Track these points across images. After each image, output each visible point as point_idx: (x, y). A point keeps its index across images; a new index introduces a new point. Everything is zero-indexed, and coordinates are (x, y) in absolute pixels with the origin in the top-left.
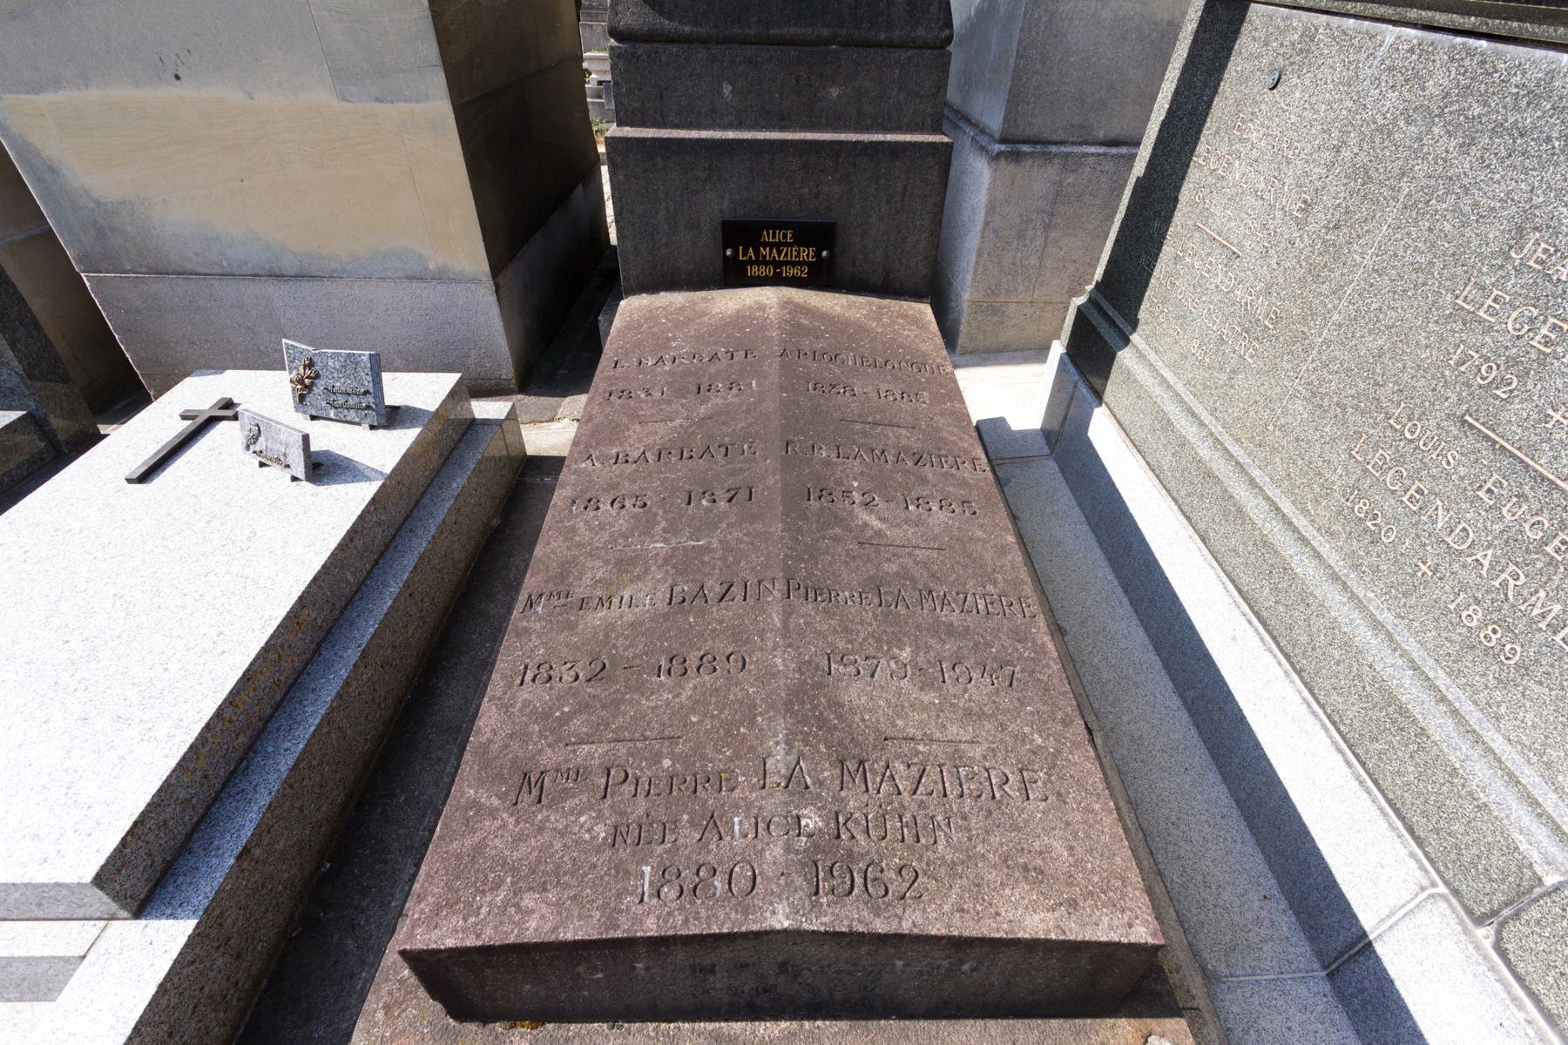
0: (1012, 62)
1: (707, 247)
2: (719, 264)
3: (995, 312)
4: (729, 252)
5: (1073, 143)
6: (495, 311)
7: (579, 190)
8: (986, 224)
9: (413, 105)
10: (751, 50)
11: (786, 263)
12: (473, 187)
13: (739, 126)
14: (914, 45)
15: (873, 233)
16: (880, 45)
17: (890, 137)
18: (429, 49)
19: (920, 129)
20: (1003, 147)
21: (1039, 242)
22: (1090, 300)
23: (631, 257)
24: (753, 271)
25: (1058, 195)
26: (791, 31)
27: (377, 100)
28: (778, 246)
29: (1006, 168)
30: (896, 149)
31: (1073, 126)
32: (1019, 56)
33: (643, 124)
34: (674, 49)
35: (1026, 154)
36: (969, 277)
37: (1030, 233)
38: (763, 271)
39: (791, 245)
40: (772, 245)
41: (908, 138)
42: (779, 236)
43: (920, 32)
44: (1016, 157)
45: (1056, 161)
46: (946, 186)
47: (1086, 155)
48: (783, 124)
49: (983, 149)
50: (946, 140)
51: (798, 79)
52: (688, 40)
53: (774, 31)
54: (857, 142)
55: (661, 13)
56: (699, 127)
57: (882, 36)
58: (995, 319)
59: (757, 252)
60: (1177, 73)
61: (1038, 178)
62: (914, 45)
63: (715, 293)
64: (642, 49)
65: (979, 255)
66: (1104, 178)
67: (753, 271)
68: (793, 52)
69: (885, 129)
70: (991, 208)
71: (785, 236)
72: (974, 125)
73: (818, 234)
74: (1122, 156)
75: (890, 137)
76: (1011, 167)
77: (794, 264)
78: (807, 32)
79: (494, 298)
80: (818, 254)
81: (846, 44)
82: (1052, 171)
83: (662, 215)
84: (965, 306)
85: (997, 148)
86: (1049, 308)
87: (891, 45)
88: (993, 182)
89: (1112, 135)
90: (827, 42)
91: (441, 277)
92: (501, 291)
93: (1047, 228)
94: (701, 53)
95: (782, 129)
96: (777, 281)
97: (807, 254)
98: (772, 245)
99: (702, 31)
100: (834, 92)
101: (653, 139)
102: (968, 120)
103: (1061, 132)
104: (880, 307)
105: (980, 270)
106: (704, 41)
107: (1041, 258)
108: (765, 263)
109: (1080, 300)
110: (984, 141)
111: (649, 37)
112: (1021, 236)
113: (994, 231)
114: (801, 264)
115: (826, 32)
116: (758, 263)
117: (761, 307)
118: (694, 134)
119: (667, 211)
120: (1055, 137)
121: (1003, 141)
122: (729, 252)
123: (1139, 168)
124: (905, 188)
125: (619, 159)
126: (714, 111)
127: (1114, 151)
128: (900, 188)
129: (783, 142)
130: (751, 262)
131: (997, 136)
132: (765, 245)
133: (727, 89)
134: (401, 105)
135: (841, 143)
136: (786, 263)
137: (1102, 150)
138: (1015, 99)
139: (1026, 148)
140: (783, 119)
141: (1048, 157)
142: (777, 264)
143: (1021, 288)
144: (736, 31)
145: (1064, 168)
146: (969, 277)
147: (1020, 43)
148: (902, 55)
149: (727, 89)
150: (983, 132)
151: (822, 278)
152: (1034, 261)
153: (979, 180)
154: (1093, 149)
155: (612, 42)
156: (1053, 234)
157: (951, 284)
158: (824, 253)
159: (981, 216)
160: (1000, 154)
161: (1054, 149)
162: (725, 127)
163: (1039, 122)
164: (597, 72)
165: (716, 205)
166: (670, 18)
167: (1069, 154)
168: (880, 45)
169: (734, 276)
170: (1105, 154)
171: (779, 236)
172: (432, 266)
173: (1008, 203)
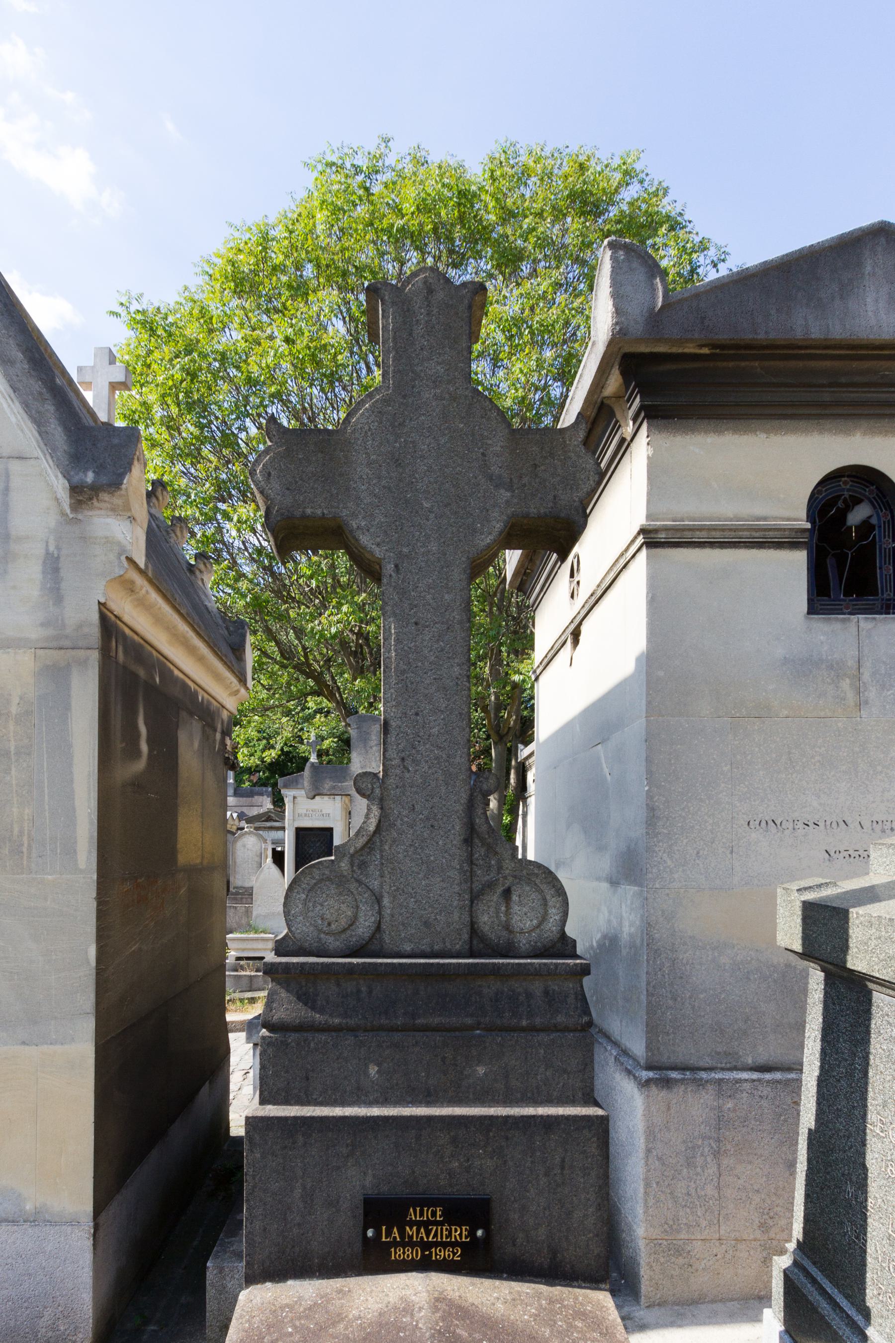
0: (643, 998)
1: (344, 1225)
2: (358, 1246)
3: (679, 1252)
4: (370, 1233)
5: (723, 1069)
6: (87, 1258)
7: (206, 1089)
8: (648, 1151)
9: (58, 1048)
10: (397, 1037)
11: (436, 1244)
12: (95, 1122)
13: (385, 1102)
14: (556, 1028)
15: (533, 1208)
16: (523, 1029)
17: (542, 1111)
18: (87, 1000)
19: (573, 1102)
20: (651, 1074)
21: (712, 1170)
22: (796, 1263)
23: (258, 1239)
24: (397, 1254)
25: (720, 1121)
26: (436, 1020)
27: (24, 1043)
28: (426, 1224)
29: (659, 1095)
30: (549, 1123)
31: (718, 1053)
32: (649, 994)
33: (287, 1102)
34: (323, 1037)
35: (676, 1081)
36: (640, 1210)
37: (699, 1161)
38: (411, 1254)
39: (441, 1223)
40: (419, 1224)
41: (560, 1111)
42: (427, 1214)
43: (560, 1019)
44: (666, 1083)
45: (710, 1087)
46: (608, 1162)
47: (739, 1081)
48: (429, 1099)
49: (629, 1072)
50: (600, 1112)
51: (444, 1059)
52: (338, 1029)
53: (418, 1021)
54: (507, 1117)
55: (313, 1008)
56: (343, 1104)
57: (524, 1023)
58: (681, 1261)
59: (402, 1233)
60: (818, 1046)
61: (695, 1105)
62: (556, 1028)
63: (353, 1282)
64: (292, 1037)
65: (647, 1185)
66: (764, 1103)
67: (397, 1254)
68: (438, 1037)
69: (536, 1103)
70: (651, 1134)
71: (434, 1214)
72: (616, 1044)
73: (471, 1210)
74: (778, 1082)
75: (542, 1111)
76: (664, 1093)
77: (444, 1245)
78: (454, 1021)
79: (89, 1243)
80: (472, 1233)
81: (489, 1029)
82: (708, 1096)
83: (298, 1193)
84: (642, 1244)
85: (645, 1075)
86: (742, 1246)
87: (533, 1029)
88: (648, 1108)
89: (762, 1059)
90: (472, 1028)
91: (37, 1219)
92: (101, 1233)
93: (717, 1154)
94: (350, 1040)
95: (428, 1104)
96: (425, 1265)
97: (460, 1233)
98: (419, 1224)
99: (352, 1022)
100: (481, 1070)
101: (295, 1118)
102: (608, 1037)
103: (707, 1059)
104: (551, 1301)
105: (651, 1202)
106: (352, 1030)
107: (718, 1188)
108: (412, 1244)
109: (784, 1262)
110: (629, 1064)
111: (299, 1028)
112: (690, 1164)
113: (659, 1159)
114: (454, 1244)
115: (469, 1021)
116: (403, 1244)
117: (408, 1309)
118: (338, 1112)
119: (304, 1187)
120: (701, 1064)
121: (649, 1068)
122: (370, 1233)
123: (808, 1118)
124: (563, 1161)
125: (257, 1137)
126: (358, 1089)
127: (768, 1076)
128: (558, 1159)
129: (430, 1119)
130: (395, 1244)
131: (642, 1062)
132: (411, 1224)
133: (373, 1070)
134: (45, 1048)
135: (491, 1118)
136: (436, 1244)
137: (755, 1075)
138: (653, 1031)
139: (674, 1075)
140: (429, 1094)
141: (701, 1084)
142: (426, 1246)
143: (704, 1224)
144: (384, 1021)
145: (719, 1094)
146: (640, 1210)
147: (648, 983)
148: (544, 1037)
149: (373, 1070)
150: (625, 1052)
151: (478, 1261)
152: (710, 1190)
153: (631, 1108)
154: (745, 1075)
155: (264, 1032)
156: (725, 1162)
157: (619, 1210)
158: (480, 1233)
159: (640, 1142)
160: (648, 1082)
161: (704, 1075)
162: (370, 1104)
163: (684, 1050)
164: (236, 950)
165: (358, 1180)
166: (321, 1011)
167: (721, 1080)
168: (523, 1029)
169: (375, 1260)
170: (759, 1080)
171: (427, 1214)
172: (28, 1207)
173: (669, 1129)
